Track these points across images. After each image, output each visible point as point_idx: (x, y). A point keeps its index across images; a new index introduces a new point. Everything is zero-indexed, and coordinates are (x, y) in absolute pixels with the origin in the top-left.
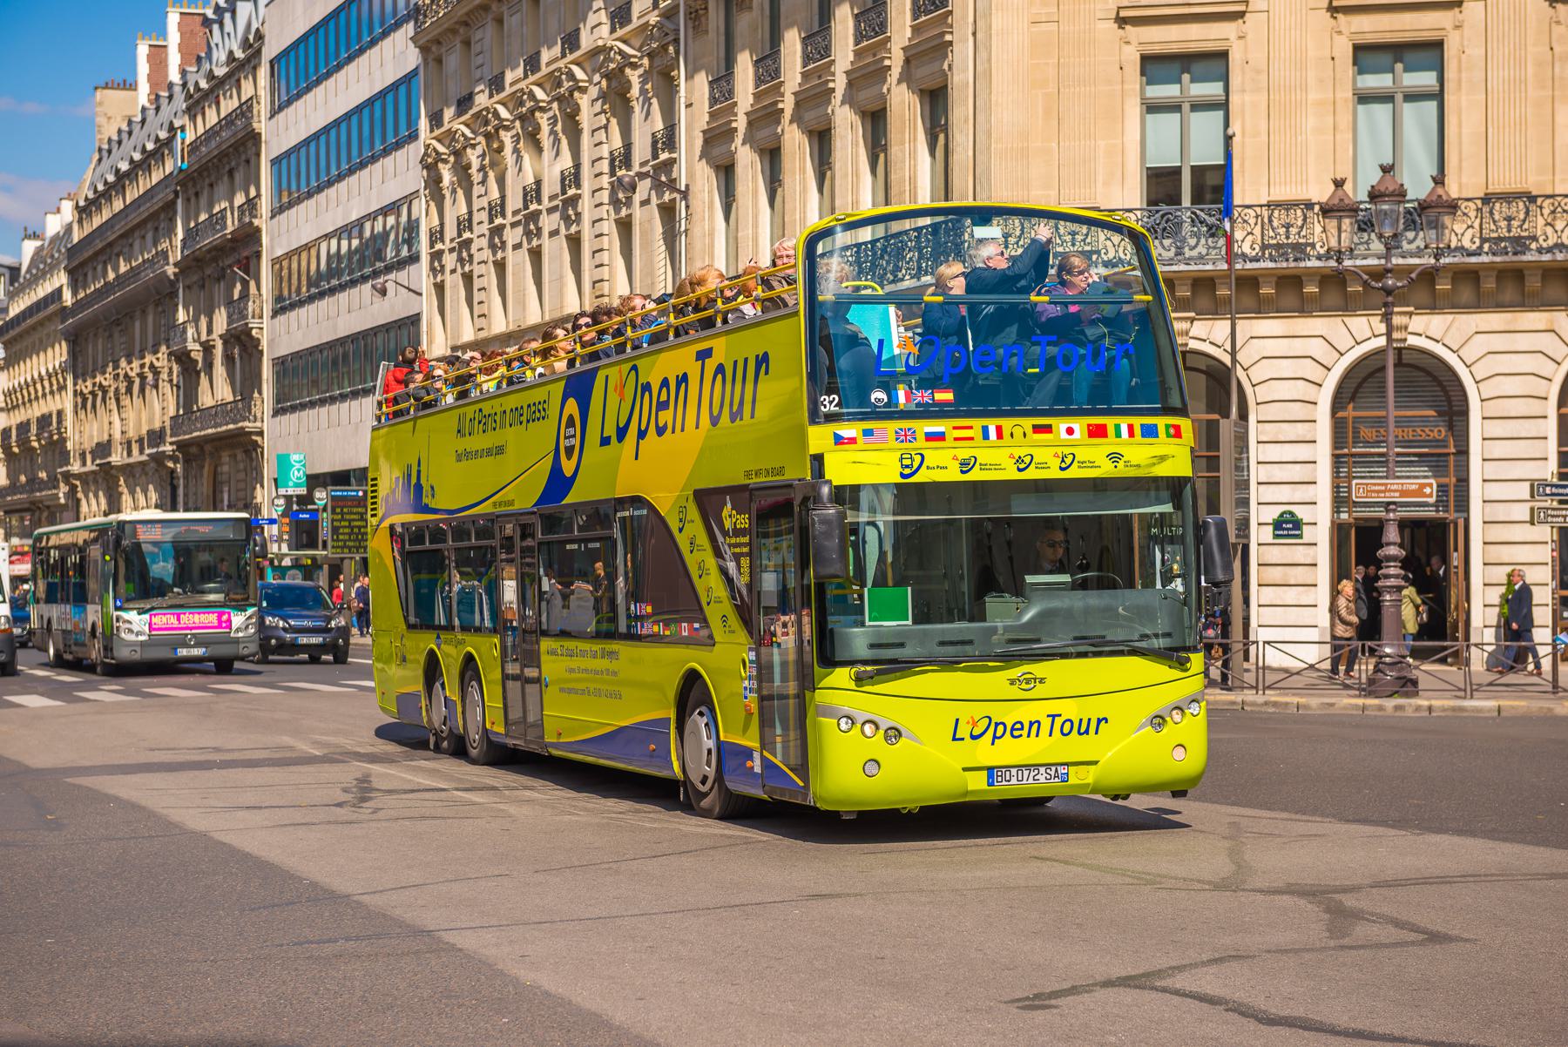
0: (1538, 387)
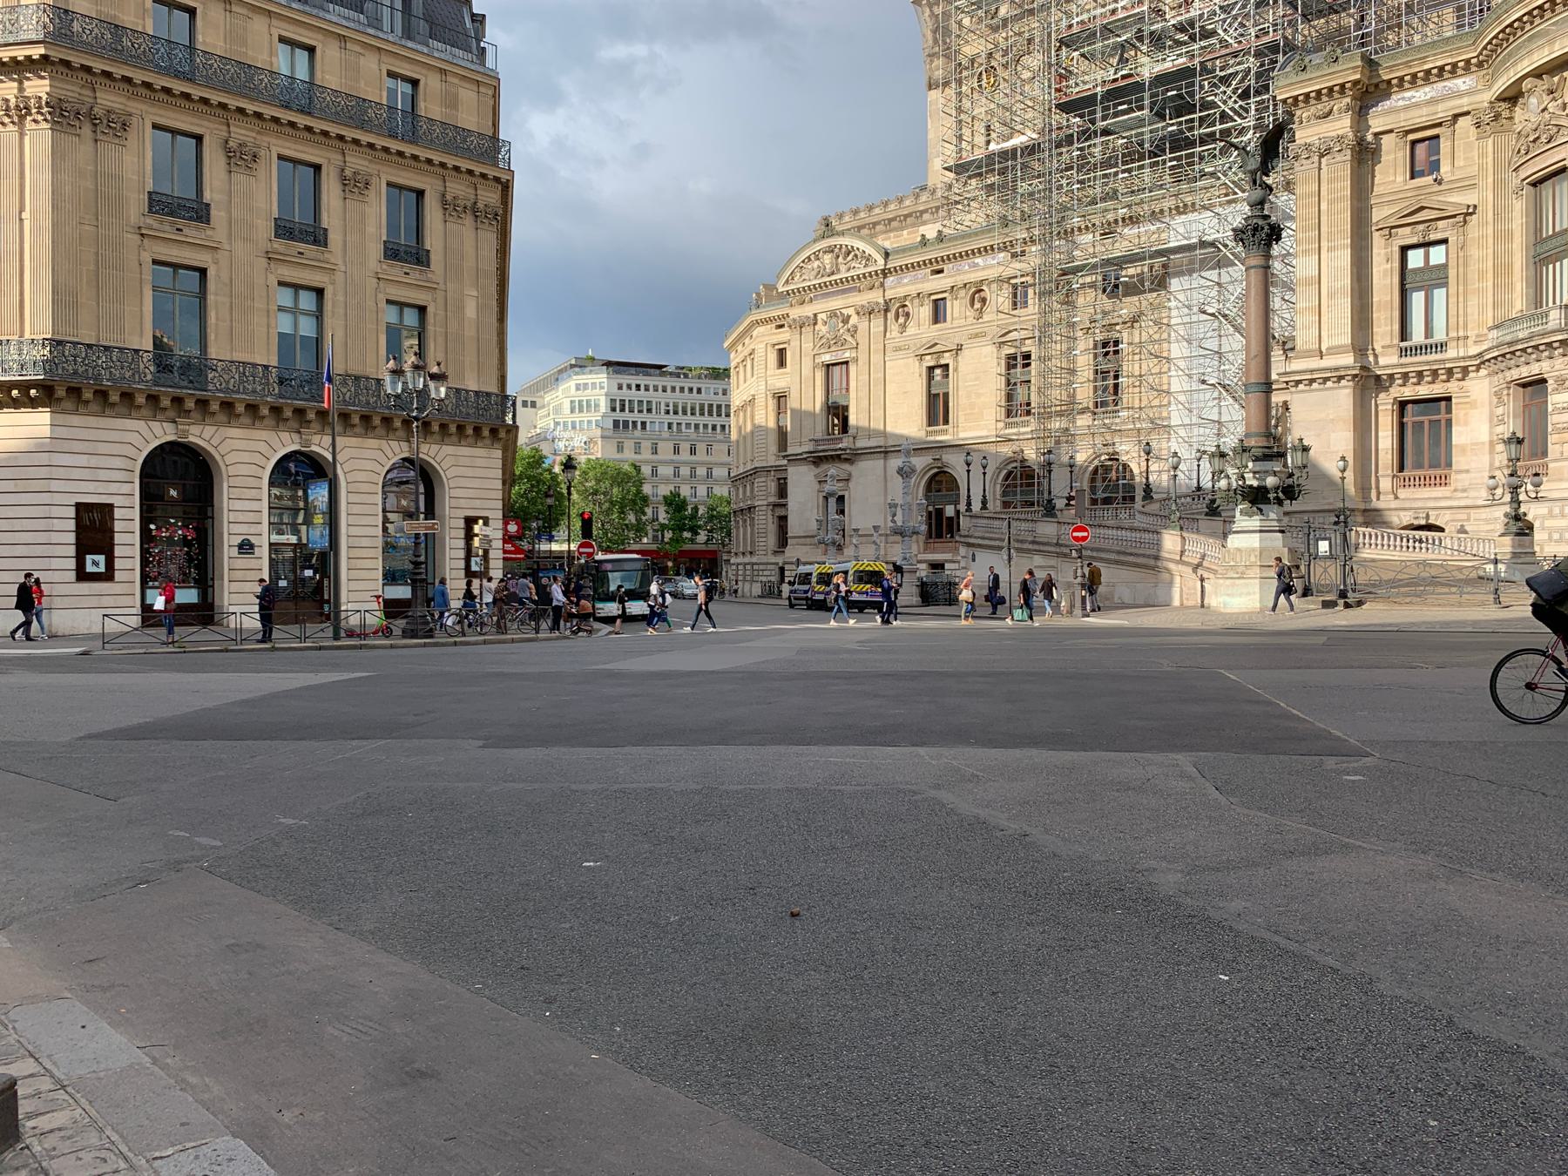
0: (259, 472)
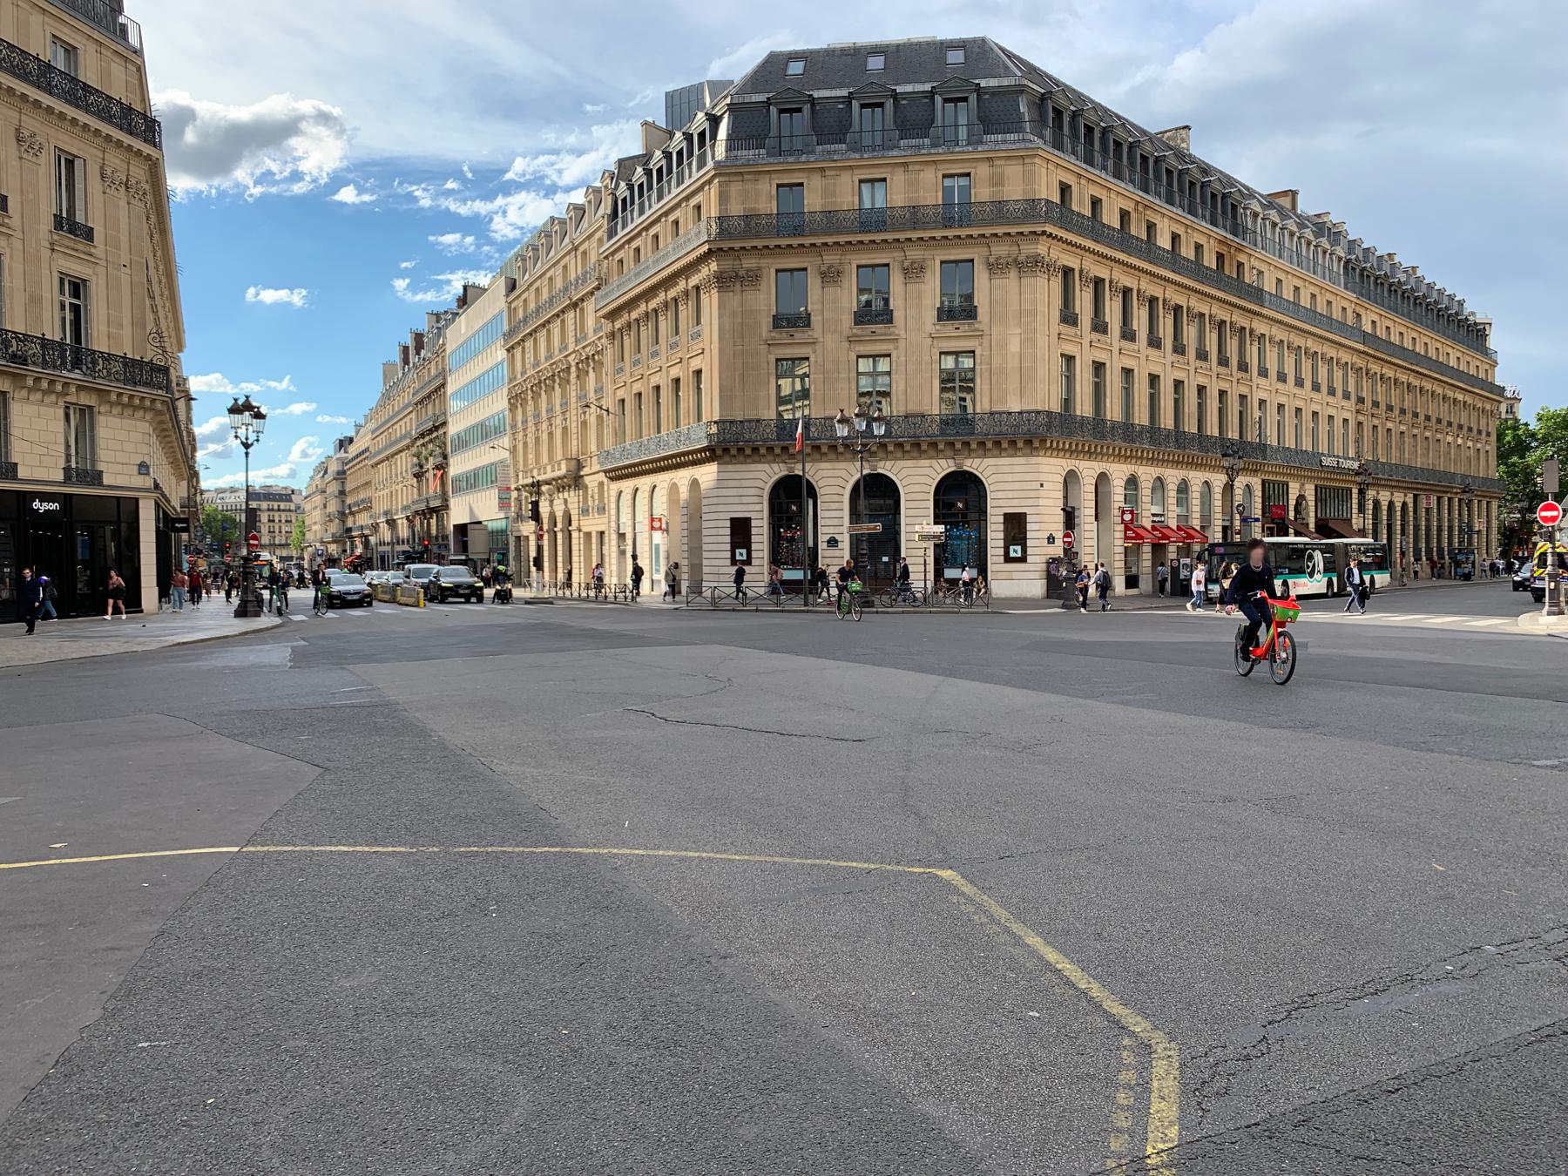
0: (840, 491)
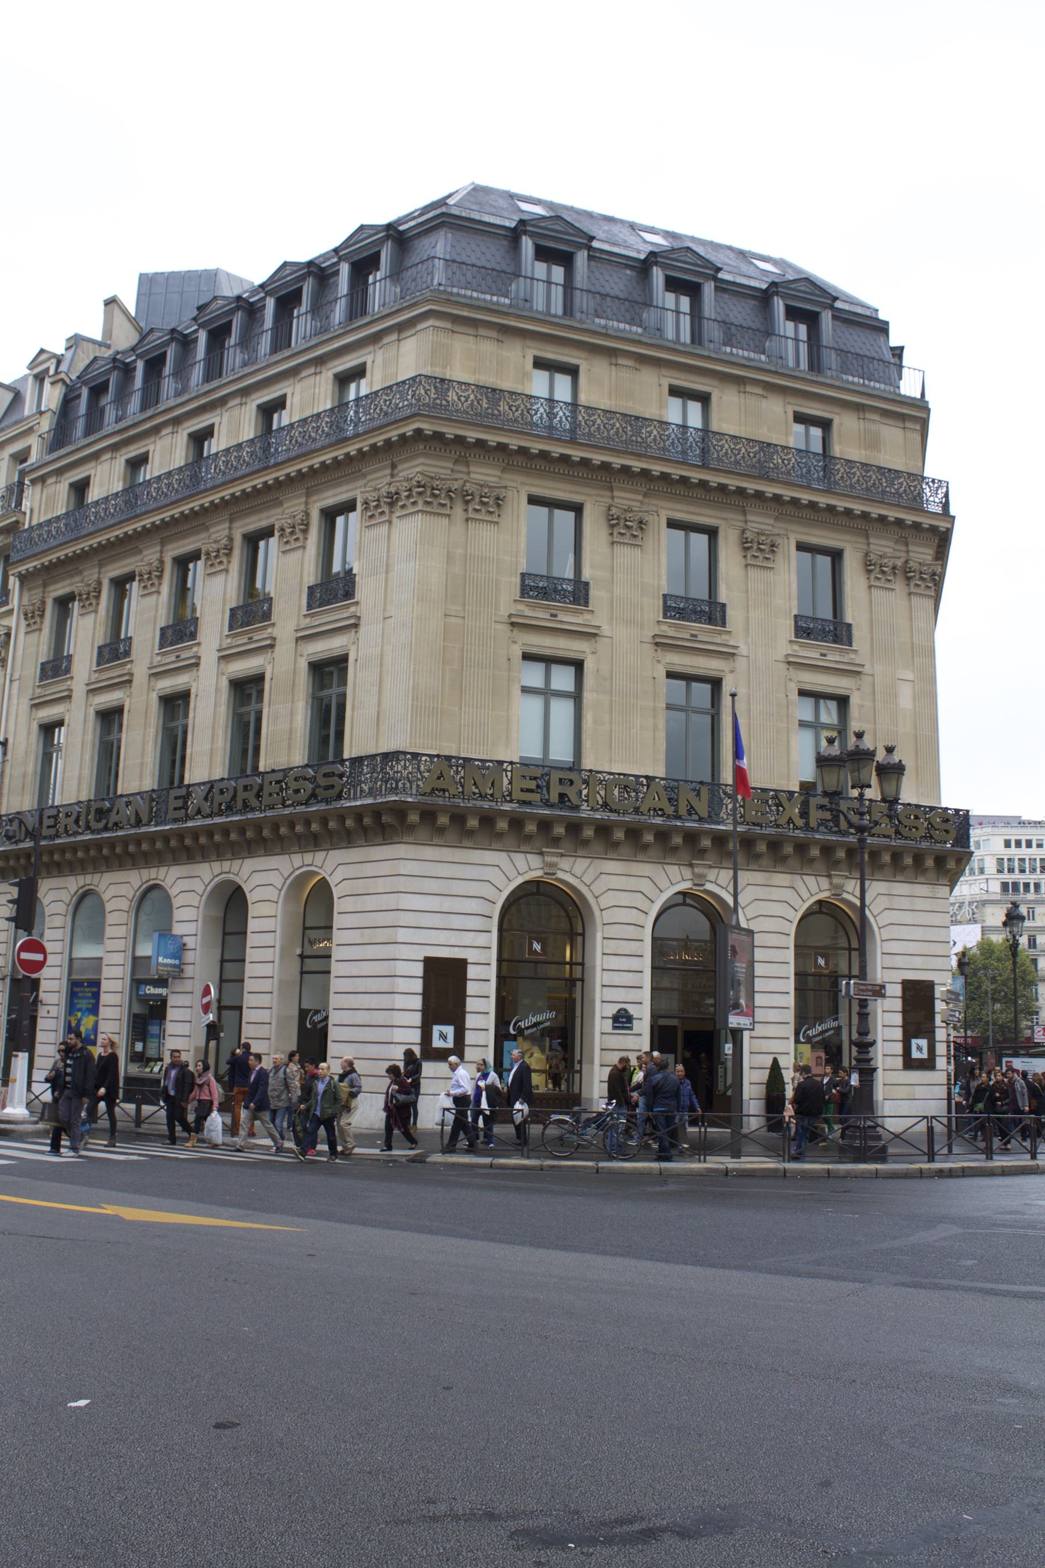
0: (639, 918)
